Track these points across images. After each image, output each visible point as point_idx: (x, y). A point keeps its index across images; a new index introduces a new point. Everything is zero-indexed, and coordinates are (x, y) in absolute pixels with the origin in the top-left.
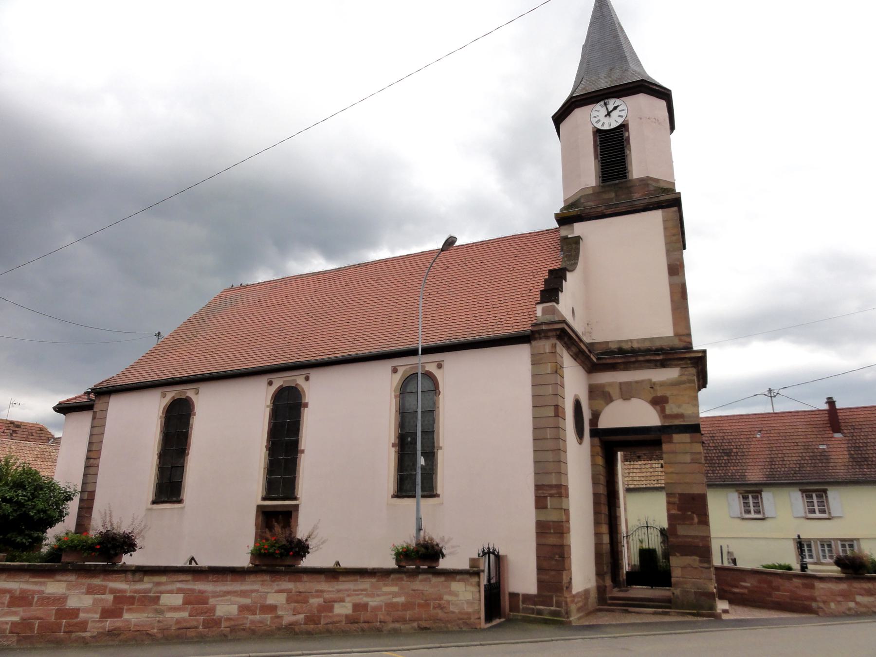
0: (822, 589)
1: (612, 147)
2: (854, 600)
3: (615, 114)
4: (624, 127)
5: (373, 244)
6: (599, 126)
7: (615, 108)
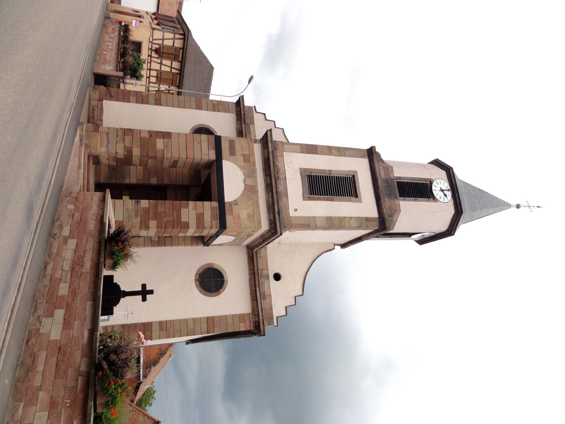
0: (92, 199)
1: (420, 190)
2: (71, 236)
3: (441, 194)
4: (434, 198)
5: (390, 230)
6: (434, 184)
7: (445, 195)
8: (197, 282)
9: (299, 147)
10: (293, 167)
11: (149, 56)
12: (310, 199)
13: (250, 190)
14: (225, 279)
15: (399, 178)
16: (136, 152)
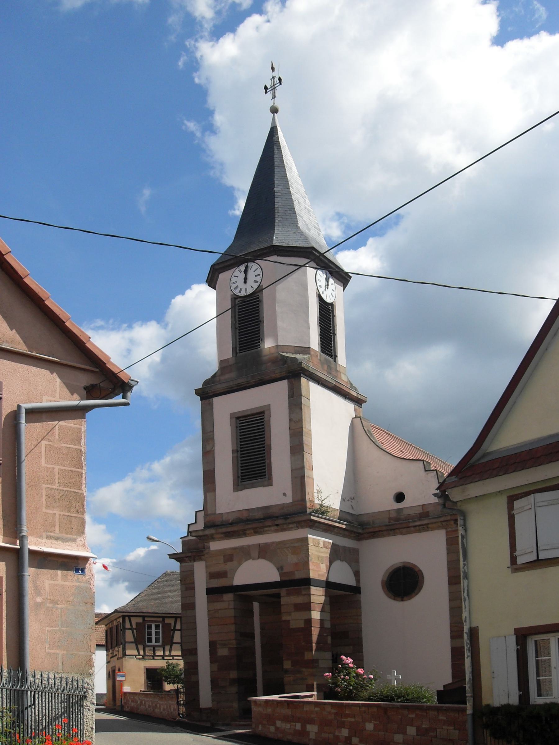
4: (260, 290)
8: (405, 598)
9: (208, 494)
10: (234, 501)
11: (163, 658)
12: (270, 478)
13: (264, 552)
14: (401, 565)
15: (234, 349)
16: (233, 674)
